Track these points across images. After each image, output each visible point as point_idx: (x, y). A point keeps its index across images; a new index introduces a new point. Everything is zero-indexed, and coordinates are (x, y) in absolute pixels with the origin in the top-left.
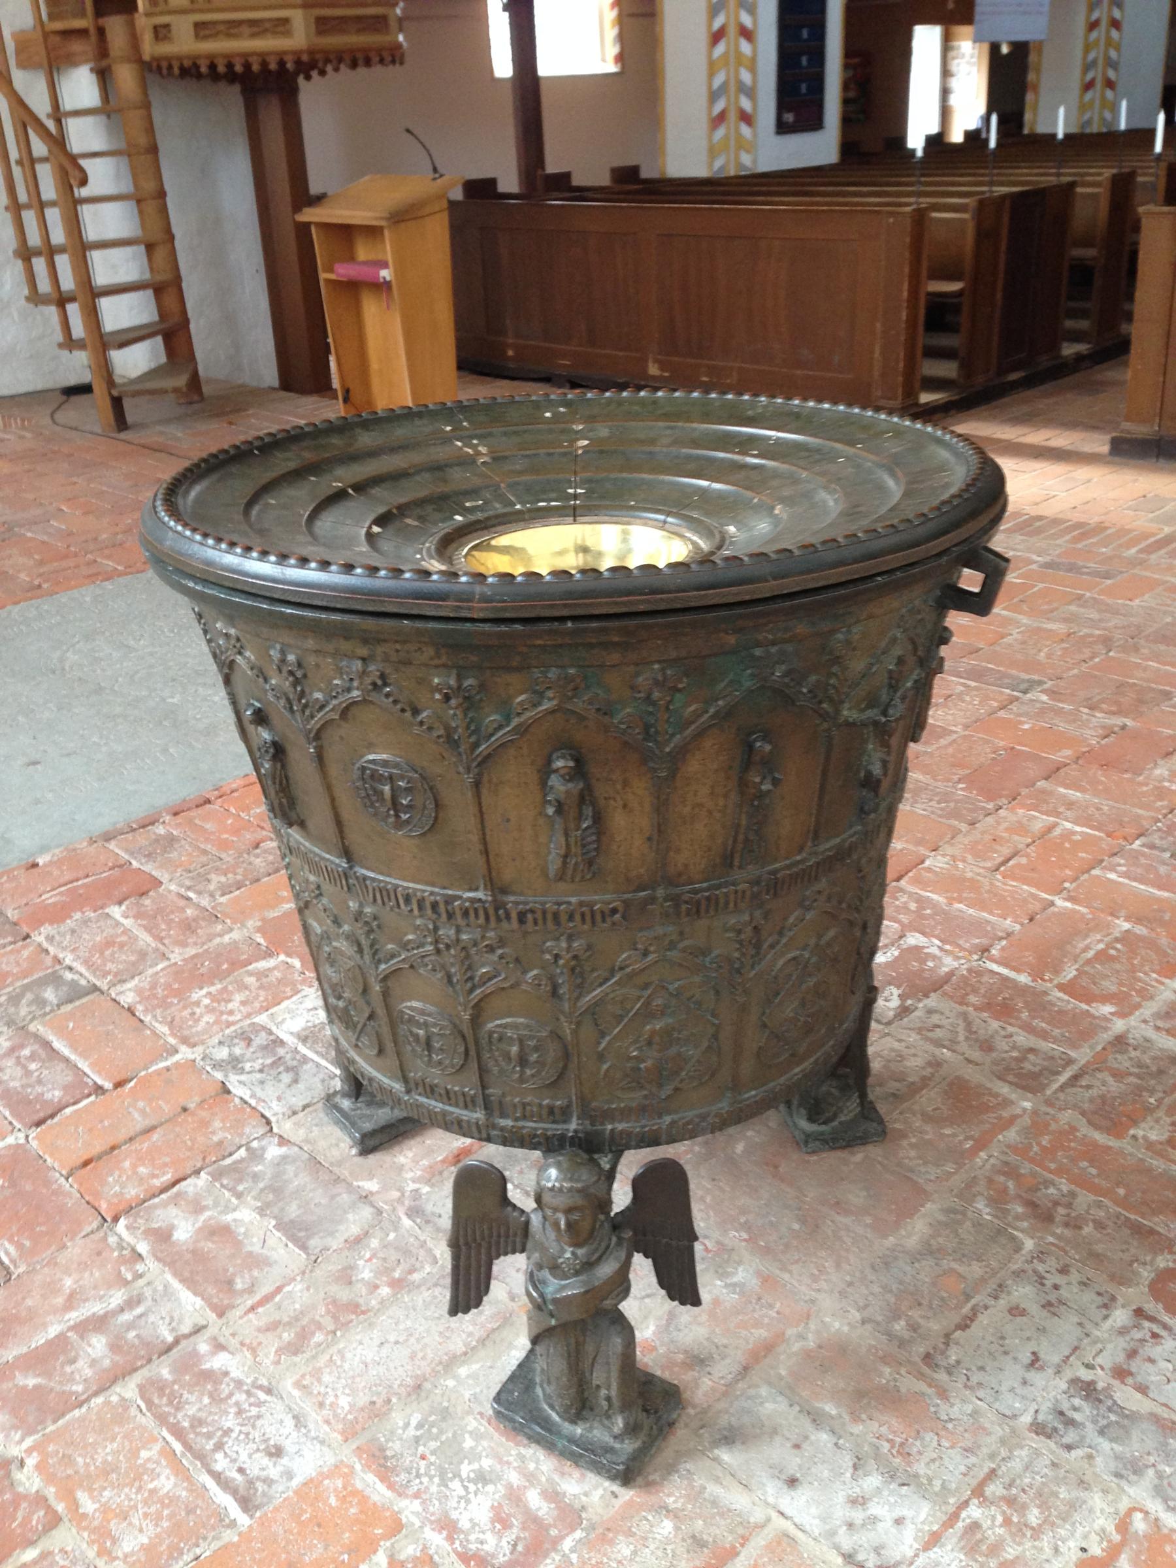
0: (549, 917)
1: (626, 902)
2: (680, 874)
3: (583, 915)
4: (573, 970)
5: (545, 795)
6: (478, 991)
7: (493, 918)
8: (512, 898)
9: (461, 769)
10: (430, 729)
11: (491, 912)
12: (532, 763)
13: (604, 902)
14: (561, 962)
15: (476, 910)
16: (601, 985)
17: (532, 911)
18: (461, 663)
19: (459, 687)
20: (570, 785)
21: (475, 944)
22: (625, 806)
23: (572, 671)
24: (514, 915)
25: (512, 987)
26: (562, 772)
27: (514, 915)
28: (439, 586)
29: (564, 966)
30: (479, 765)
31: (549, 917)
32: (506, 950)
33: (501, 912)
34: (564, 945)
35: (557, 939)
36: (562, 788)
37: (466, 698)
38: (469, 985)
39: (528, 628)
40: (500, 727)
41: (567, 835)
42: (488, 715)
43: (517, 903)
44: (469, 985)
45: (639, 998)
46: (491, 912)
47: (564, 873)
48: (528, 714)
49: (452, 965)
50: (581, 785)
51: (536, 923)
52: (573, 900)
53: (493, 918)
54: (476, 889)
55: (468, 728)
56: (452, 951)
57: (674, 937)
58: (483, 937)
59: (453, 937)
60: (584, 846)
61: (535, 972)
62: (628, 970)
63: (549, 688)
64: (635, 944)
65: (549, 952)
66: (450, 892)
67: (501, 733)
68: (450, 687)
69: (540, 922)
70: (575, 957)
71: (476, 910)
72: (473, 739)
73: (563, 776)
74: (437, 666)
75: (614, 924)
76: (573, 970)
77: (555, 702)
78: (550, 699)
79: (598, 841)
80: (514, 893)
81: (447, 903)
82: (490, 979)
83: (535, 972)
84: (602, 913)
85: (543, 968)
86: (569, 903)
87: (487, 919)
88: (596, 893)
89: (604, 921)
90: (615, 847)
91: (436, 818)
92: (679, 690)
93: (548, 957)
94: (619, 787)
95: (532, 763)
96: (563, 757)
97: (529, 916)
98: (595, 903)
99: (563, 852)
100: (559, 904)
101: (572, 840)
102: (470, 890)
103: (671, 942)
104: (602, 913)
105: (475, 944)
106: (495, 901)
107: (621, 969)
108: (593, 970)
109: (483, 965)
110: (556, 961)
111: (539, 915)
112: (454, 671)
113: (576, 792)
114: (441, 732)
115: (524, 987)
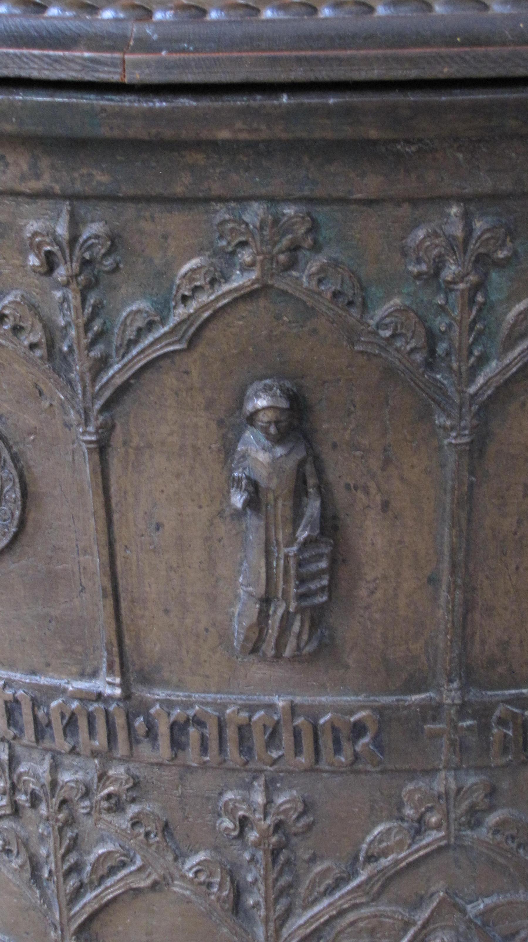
0: (231, 733)
1: (380, 710)
2: (492, 663)
3: (297, 734)
4: (275, 853)
5: (231, 470)
6: (89, 896)
7: (122, 735)
8: (161, 694)
9: (73, 416)
10: (17, 330)
11: (120, 721)
12: (209, 405)
13: (338, 709)
14: (253, 836)
15: (91, 718)
16: (329, 891)
17: (199, 723)
18: (78, 187)
19: (73, 240)
20: (279, 451)
21: (87, 794)
22: (386, 506)
23: (289, 211)
24: (163, 729)
25: (154, 886)
26: (264, 418)
27: (163, 729)
28: (60, 24)
29: (257, 845)
30: (107, 407)
31: (231, 733)
32: (148, 807)
33: (139, 722)
34: (259, 798)
35: (248, 787)
36: (263, 457)
37: (85, 263)
38: (73, 882)
39: (205, 135)
40: (150, 326)
41: (268, 553)
42: (125, 304)
43: (169, 704)
44: (73, 882)
45: (407, 925)
46: (120, 721)
47: (261, 639)
48: (204, 298)
49: (42, 838)
50: (300, 454)
51: (204, 748)
52: (281, 702)
53: (122, 735)
54: (94, 675)
55: (87, 327)
56: (43, 810)
57: (478, 796)
58: (102, 776)
59: (46, 778)
60: (302, 580)
61: (201, 856)
62: (384, 862)
63: (243, 244)
64: (400, 806)
65: (231, 813)
66: (43, 680)
67: (150, 339)
68: (56, 241)
69: (214, 745)
70: (278, 826)
71: (91, 718)
72: (96, 352)
73: (265, 430)
74: (34, 196)
75: (356, 757)
76: (275, 853)
77: (253, 276)
78: (246, 268)
79: (332, 571)
80: (165, 684)
81: (35, 703)
82: (112, 871)
83: (201, 856)
84: (335, 730)
85: (216, 848)
86: (271, 707)
87: (111, 737)
88: (323, 688)
89: (338, 749)
90: (363, 593)
91: (22, 523)
92: (500, 265)
93: (227, 823)
94: (375, 464)
95: (209, 405)
96: (267, 389)
97: (193, 731)
98: (323, 709)
99: (261, 590)
100: (252, 709)
101: (279, 565)
102: (82, 675)
103: (472, 810)
104: (335, 730)
105: (87, 794)
106: (127, 696)
107: (370, 858)
108: (313, 859)
109: (102, 840)
110: (241, 835)
111: (212, 732)
112: (66, 207)
113: (291, 464)
114: (38, 336)
115: (178, 887)
